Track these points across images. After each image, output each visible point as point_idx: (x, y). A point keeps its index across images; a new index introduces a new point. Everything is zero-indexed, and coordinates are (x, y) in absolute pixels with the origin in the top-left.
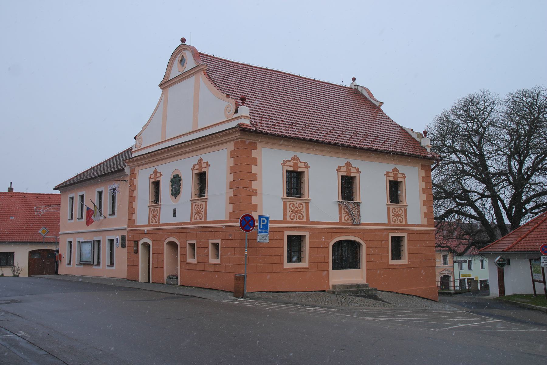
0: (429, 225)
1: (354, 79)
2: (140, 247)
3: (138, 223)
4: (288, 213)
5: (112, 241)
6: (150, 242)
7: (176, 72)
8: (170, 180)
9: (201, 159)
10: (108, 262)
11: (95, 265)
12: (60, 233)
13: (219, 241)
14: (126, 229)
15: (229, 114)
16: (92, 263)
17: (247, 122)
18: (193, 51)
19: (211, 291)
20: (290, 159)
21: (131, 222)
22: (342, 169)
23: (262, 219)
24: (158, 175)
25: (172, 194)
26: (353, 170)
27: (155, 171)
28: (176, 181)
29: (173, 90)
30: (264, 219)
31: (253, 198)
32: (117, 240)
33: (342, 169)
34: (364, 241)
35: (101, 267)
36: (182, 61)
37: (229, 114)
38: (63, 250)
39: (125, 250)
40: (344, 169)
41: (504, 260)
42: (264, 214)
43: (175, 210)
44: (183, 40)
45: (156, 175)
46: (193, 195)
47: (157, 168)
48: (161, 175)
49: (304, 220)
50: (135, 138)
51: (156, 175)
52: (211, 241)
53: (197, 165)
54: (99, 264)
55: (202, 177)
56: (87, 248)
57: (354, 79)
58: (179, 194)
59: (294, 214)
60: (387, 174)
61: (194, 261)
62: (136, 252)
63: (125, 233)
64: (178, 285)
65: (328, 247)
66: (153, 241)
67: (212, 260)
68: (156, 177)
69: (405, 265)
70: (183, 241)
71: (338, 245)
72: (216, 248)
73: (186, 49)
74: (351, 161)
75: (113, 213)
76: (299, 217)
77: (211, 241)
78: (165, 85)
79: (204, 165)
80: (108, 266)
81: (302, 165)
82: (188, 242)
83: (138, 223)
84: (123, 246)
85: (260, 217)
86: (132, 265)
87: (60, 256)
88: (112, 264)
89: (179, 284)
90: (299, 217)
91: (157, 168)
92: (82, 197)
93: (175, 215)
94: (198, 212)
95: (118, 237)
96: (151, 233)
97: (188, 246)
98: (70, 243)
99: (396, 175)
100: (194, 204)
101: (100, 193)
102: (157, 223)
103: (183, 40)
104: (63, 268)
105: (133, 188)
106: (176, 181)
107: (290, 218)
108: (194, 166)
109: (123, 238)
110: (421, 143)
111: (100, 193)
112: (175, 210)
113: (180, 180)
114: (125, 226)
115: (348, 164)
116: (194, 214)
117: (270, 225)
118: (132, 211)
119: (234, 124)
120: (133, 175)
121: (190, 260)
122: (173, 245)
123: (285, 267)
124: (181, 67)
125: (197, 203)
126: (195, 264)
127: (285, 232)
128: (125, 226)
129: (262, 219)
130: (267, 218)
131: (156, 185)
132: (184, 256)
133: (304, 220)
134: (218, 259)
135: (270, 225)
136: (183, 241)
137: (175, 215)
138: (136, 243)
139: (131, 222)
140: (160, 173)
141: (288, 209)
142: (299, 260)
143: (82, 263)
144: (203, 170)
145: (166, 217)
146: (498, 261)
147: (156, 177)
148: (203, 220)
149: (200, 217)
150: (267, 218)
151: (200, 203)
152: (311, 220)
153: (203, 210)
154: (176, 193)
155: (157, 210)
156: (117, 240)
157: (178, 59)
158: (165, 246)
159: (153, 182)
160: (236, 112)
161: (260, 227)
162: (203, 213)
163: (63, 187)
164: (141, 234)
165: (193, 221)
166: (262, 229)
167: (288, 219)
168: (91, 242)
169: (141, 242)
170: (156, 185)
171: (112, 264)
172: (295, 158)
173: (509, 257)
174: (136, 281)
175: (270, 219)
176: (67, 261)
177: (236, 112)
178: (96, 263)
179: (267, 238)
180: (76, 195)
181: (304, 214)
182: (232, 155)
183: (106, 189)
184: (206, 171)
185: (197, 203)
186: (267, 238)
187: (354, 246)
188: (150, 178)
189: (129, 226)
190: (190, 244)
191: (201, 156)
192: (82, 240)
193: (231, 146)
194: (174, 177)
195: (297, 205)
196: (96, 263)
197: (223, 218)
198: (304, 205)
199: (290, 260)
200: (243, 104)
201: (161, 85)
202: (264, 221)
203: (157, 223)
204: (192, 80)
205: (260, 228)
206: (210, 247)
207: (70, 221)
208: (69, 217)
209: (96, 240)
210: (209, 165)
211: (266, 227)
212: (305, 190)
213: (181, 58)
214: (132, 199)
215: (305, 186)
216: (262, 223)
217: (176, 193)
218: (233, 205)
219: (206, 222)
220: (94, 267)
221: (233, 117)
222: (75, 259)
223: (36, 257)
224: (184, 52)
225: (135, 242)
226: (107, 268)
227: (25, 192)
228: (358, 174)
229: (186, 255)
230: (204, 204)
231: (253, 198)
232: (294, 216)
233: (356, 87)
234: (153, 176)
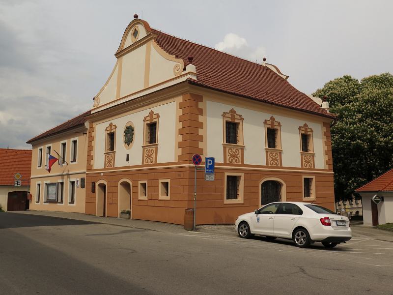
0: (329, 170)
1: (264, 60)
2: (97, 187)
3: (95, 167)
4: (228, 157)
5: (73, 183)
6: (106, 183)
7: (129, 42)
8: (123, 131)
9: (152, 112)
10: (69, 200)
11: (59, 203)
12: (31, 177)
13: (169, 181)
14: (85, 173)
15: (177, 72)
16: (56, 201)
17: (195, 78)
18: (146, 25)
19: (158, 223)
20: (229, 112)
21: (89, 167)
22: (268, 122)
23: (208, 160)
24: (113, 127)
25: (126, 143)
26: (276, 124)
27: (111, 125)
28: (129, 132)
29: (126, 58)
30: (211, 160)
31: (200, 143)
32: (77, 181)
33: (268, 122)
34: (285, 181)
35: (75, 205)
36: (135, 33)
37: (177, 72)
38: (33, 190)
39: (85, 189)
40: (269, 122)
41: (379, 198)
42: (209, 156)
43: (128, 156)
44: (136, 16)
45: (111, 128)
46: (144, 142)
47: (112, 121)
48: (116, 127)
49: (240, 163)
50: (94, 99)
51: (111, 128)
52: (160, 181)
53: (148, 117)
54: (62, 202)
55: (152, 128)
56: (53, 190)
57: (264, 60)
58: (132, 142)
59: (232, 158)
60: (300, 128)
61: (146, 198)
62: (93, 191)
63: (84, 176)
64: (130, 218)
65: (258, 186)
66: (108, 182)
67: (162, 197)
68: (111, 129)
69: (241, 204)
70: (135, 181)
71: (265, 184)
72: (165, 187)
73: (139, 23)
74: (275, 116)
75: (75, 160)
76: (236, 160)
77: (160, 181)
78: (120, 54)
79: (155, 117)
80: (70, 203)
81: (238, 117)
82: (140, 182)
83: (95, 167)
84: (83, 186)
85: (207, 159)
86: (90, 202)
87: (31, 195)
88: (72, 202)
89: (131, 218)
90: (236, 160)
91: (112, 121)
92: (49, 148)
93: (128, 160)
94: (149, 156)
95: (78, 179)
96: (106, 175)
97: (139, 185)
98: (39, 185)
99: (306, 129)
100: (146, 150)
101: (64, 145)
102: (112, 167)
103: (136, 16)
104: (33, 206)
105: (91, 139)
106: (129, 132)
107: (230, 162)
108: (145, 118)
109: (83, 180)
110: (321, 106)
111: (64, 145)
112: (128, 156)
113: (133, 130)
114: (85, 170)
115: (272, 119)
116: (145, 158)
117: (215, 166)
118: (90, 158)
119: (184, 79)
120: (92, 130)
121: (142, 197)
122: (126, 185)
123: (225, 203)
124: (134, 38)
125: (149, 149)
126: (169, 200)
127: (226, 173)
128: (85, 170)
129: (208, 160)
130: (213, 159)
131: (112, 136)
132: (136, 193)
133: (240, 163)
134: (167, 195)
135: (215, 166)
136: (135, 181)
137: (128, 160)
138: (94, 183)
139: (89, 167)
140: (115, 125)
141: (227, 154)
142: (236, 197)
143: (49, 201)
144: (154, 121)
145: (120, 161)
146: (375, 198)
147: (111, 129)
148: (154, 163)
149: (151, 160)
150: (213, 159)
151: (151, 149)
152: (245, 163)
153: (154, 154)
154: (129, 141)
155: (112, 156)
156: (77, 181)
157: (131, 32)
158: (119, 186)
159: (108, 134)
160: (185, 69)
161: (207, 167)
162: (154, 157)
163: (36, 141)
164: (98, 176)
165: (145, 163)
166: (209, 169)
167: (228, 162)
168: (55, 184)
169: (97, 184)
170: (112, 136)
171: (72, 202)
172: (232, 111)
173: (383, 196)
174: (94, 215)
175: (215, 161)
176: (36, 200)
177: (185, 69)
178: (59, 201)
179: (213, 176)
180: (45, 148)
181: (240, 158)
182: (181, 106)
183: (69, 142)
184: (156, 122)
185: (149, 149)
186: (213, 176)
187: (277, 186)
188: (106, 130)
189: (88, 170)
190: (142, 184)
191: (152, 109)
192: (48, 182)
193: (180, 99)
194: (128, 128)
195: (234, 150)
196: (59, 201)
197: (173, 160)
198: (240, 150)
199: (228, 198)
200: (191, 63)
201: (116, 55)
202: (210, 162)
203: (112, 167)
204: (144, 47)
205: (207, 169)
206: (160, 185)
207: (38, 168)
208: (38, 164)
209: (60, 183)
210: (159, 116)
211: (212, 167)
212: (239, 138)
213: (134, 31)
214: (91, 148)
215: (239, 134)
216: (208, 164)
217: (129, 141)
218: (182, 149)
219: (156, 164)
220: (58, 204)
221: (182, 74)
222: (43, 197)
223: (15, 197)
224: (137, 26)
225: (92, 183)
226: (69, 204)
227: (7, 148)
228: (279, 127)
229: (138, 193)
230: (154, 149)
231: (200, 143)
232: (232, 160)
233: (266, 65)
234: (109, 129)
